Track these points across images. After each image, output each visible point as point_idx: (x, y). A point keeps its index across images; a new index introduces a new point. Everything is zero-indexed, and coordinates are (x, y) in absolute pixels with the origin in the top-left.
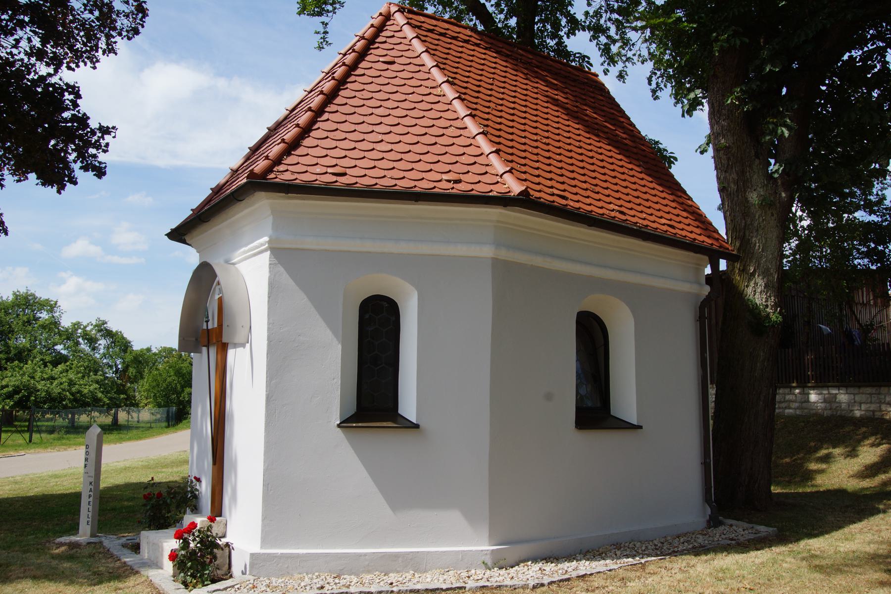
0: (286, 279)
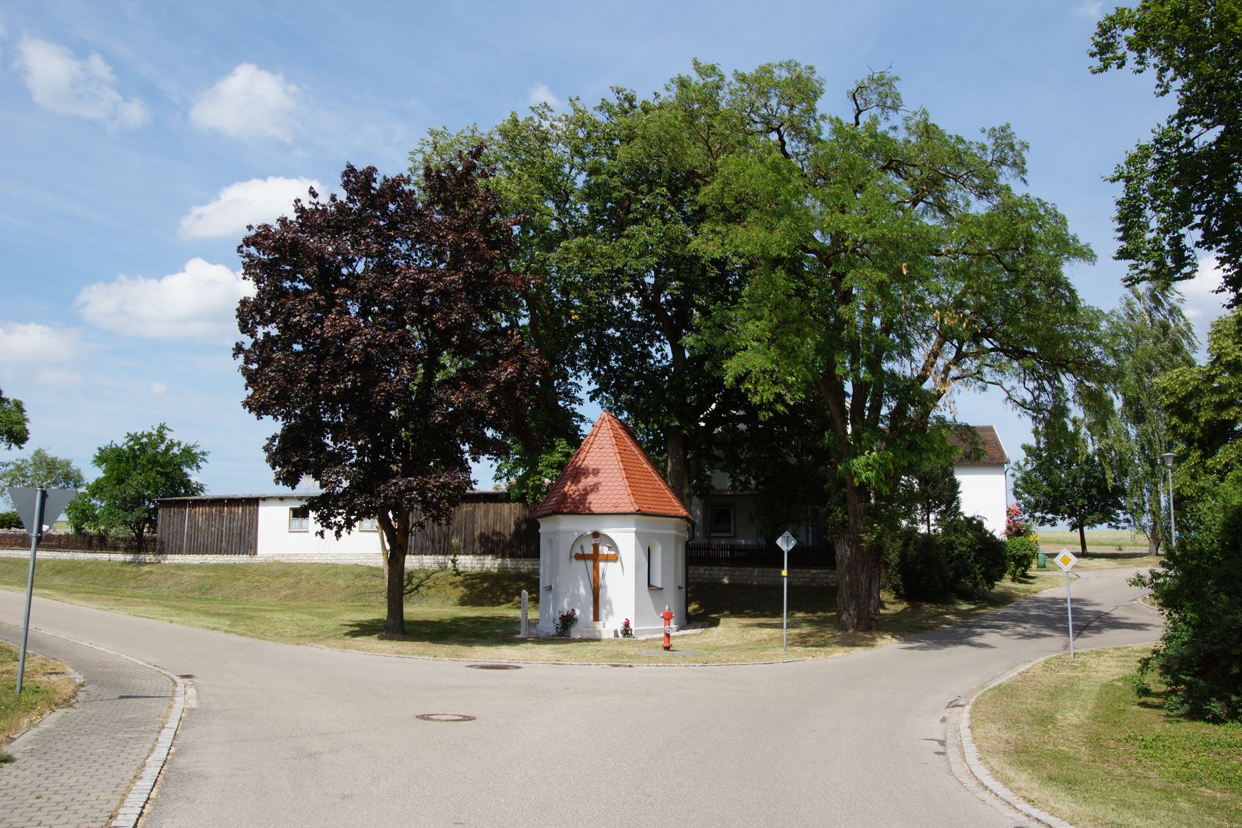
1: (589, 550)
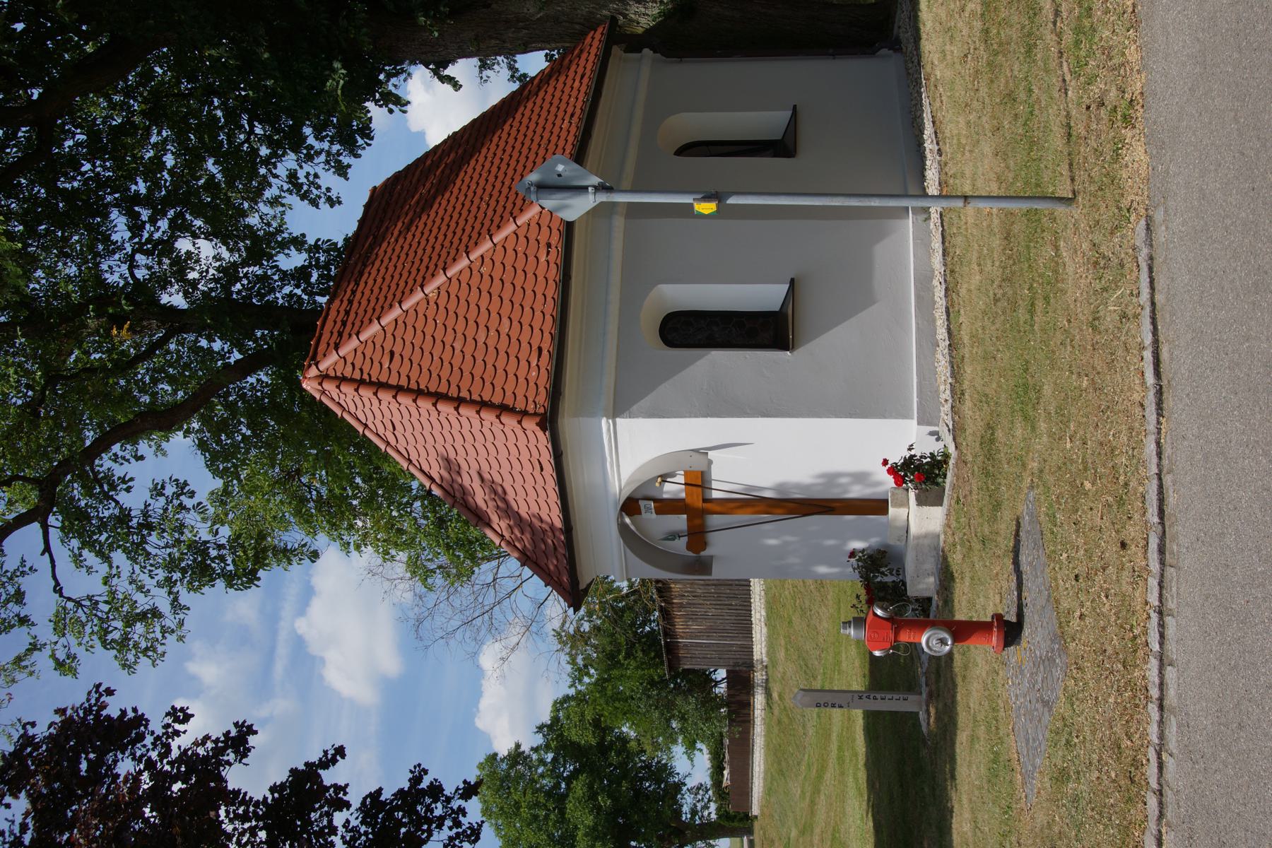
0: (645, 403)
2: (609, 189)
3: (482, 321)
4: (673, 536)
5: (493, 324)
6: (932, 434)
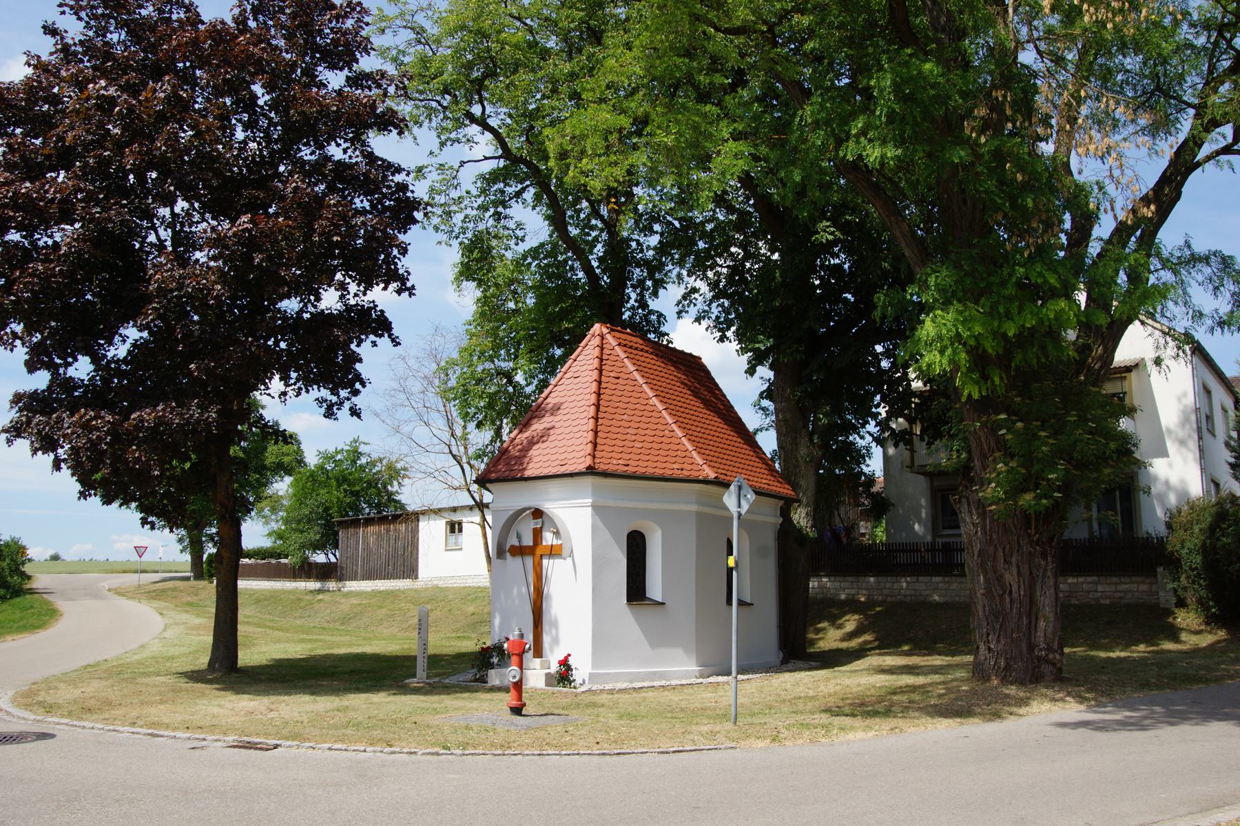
1: (528, 541)
2: (739, 518)
3: (639, 431)
4: (519, 537)
5: (638, 438)
6: (584, 681)
